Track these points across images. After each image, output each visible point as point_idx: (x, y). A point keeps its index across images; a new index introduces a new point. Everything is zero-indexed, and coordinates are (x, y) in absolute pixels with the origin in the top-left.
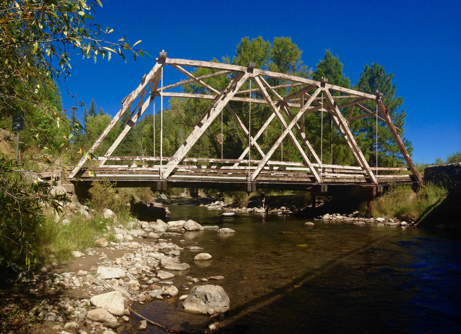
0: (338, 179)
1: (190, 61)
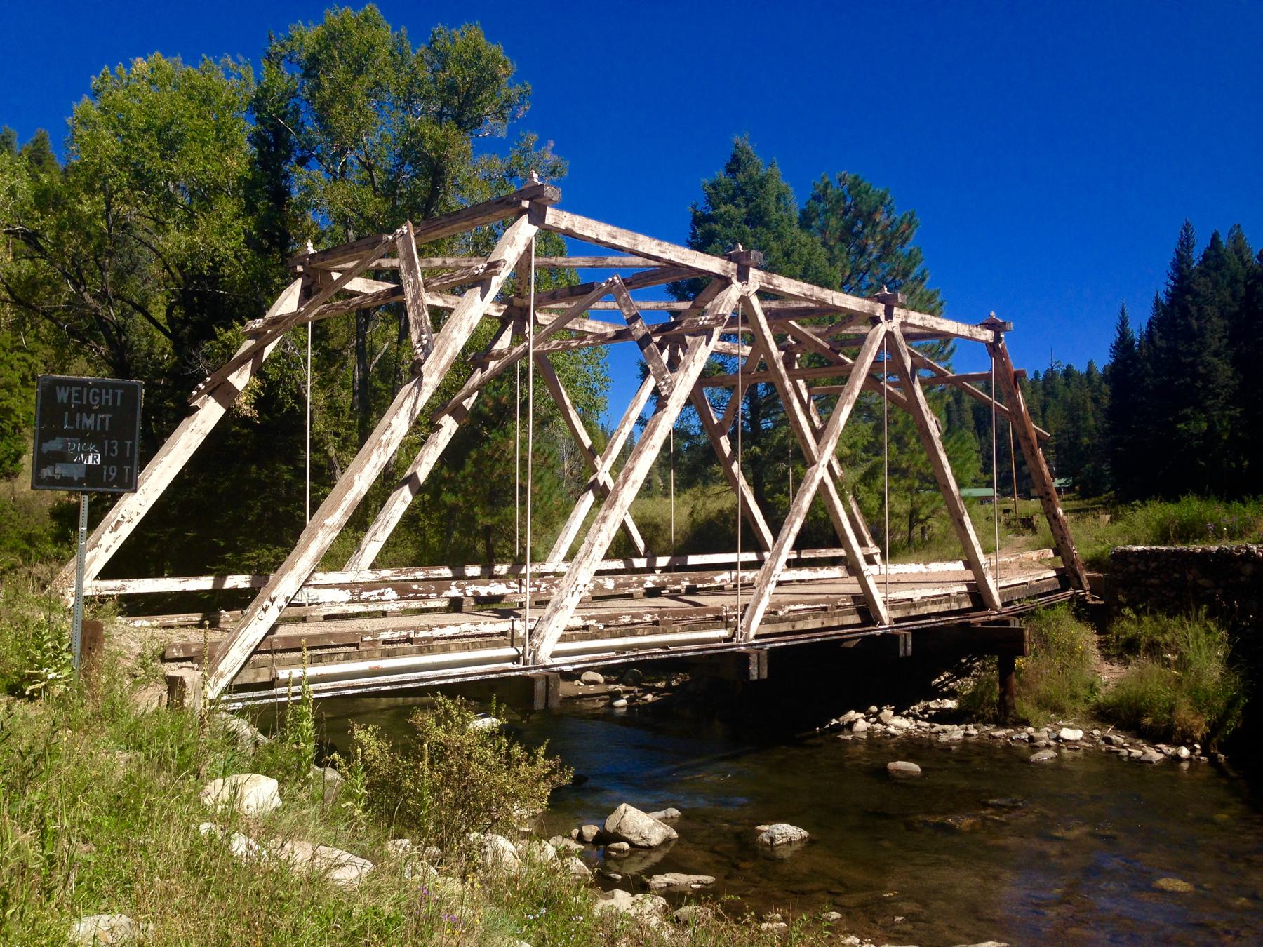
0: (914, 606)
1: (609, 228)
